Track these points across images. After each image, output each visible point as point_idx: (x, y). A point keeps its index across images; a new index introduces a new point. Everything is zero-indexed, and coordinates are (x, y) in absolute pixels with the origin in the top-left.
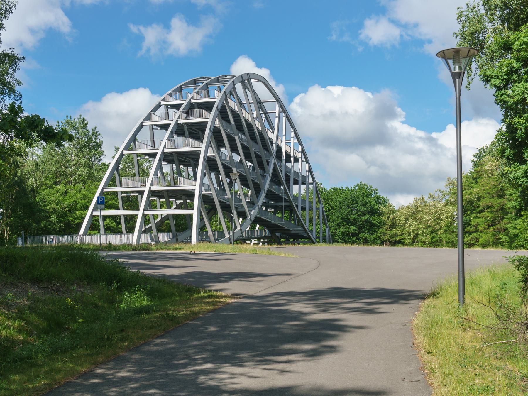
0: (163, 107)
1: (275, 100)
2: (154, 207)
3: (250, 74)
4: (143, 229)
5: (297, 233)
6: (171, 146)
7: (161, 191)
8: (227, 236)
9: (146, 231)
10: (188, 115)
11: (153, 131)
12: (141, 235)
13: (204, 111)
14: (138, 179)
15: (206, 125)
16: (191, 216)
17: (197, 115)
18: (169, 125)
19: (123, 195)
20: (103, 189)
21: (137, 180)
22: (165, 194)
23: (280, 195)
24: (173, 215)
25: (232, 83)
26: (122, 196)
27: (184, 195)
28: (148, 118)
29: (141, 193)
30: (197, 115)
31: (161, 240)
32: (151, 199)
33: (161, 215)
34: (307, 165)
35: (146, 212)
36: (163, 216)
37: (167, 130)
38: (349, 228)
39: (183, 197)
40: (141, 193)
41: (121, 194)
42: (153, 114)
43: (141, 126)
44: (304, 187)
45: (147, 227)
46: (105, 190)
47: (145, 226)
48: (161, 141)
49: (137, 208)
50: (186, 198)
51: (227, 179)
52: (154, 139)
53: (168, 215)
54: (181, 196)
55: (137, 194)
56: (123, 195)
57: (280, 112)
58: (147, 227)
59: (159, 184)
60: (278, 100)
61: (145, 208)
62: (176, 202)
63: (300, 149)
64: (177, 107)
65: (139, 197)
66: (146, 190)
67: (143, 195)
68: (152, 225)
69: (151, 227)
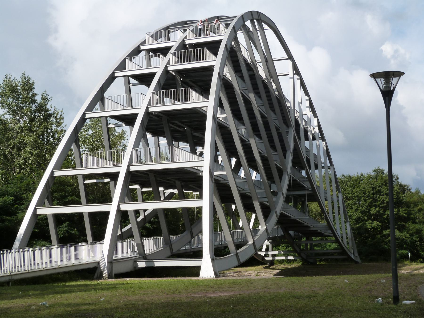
0: (143, 53)
1: (288, 58)
2: (133, 199)
3: (260, 13)
4: (119, 233)
5: (317, 231)
6: (158, 103)
7: (145, 174)
8: (251, 242)
9: (122, 238)
10: (182, 59)
11: (130, 87)
12: (115, 245)
13: (207, 51)
14: (108, 156)
15: (212, 70)
16: (200, 210)
17: (181, 96)
18: (153, 75)
19: (87, 182)
20: (53, 172)
21: (107, 158)
22: (152, 178)
23: (298, 180)
24: (166, 211)
25: (242, 19)
26: (85, 185)
27: (179, 179)
28: (122, 66)
29: (114, 176)
30: (181, 96)
31: (148, 250)
32: (131, 187)
33: (145, 211)
34: (324, 142)
35: (124, 207)
36: (147, 213)
37: (148, 85)
38: (372, 223)
39: (178, 183)
40: (114, 176)
41: (84, 180)
42: (131, 60)
43: (112, 78)
44: (323, 171)
45: (124, 230)
46: (57, 173)
47: (122, 228)
48: (143, 96)
49: (108, 200)
50: (182, 184)
51: (377, 79)
52: (130, 93)
53: (155, 212)
54: (175, 182)
55: (107, 180)
56: (87, 182)
57: (294, 74)
58: (124, 230)
59: (139, 161)
60: (290, 57)
61: (122, 200)
62: (164, 193)
63: (316, 124)
64: (164, 51)
65: (112, 184)
66: (122, 171)
67: (117, 180)
68: (132, 226)
69: (131, 229)
